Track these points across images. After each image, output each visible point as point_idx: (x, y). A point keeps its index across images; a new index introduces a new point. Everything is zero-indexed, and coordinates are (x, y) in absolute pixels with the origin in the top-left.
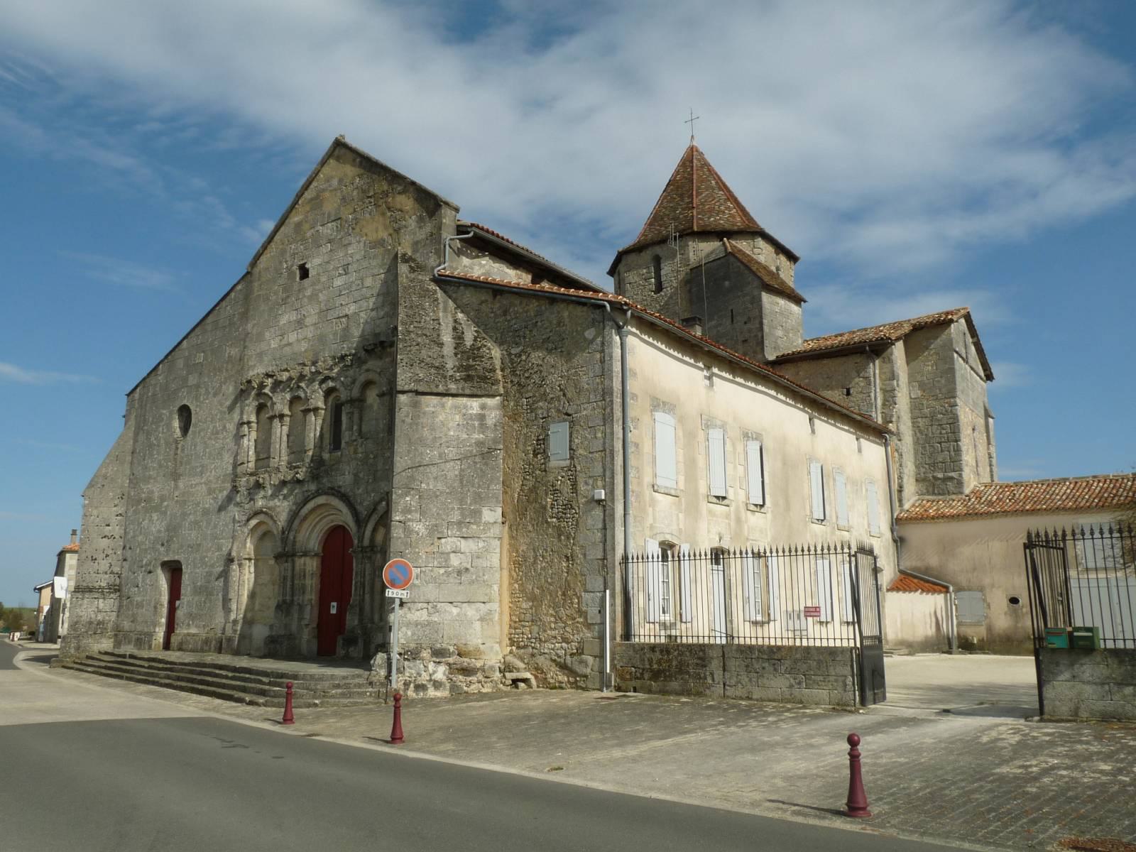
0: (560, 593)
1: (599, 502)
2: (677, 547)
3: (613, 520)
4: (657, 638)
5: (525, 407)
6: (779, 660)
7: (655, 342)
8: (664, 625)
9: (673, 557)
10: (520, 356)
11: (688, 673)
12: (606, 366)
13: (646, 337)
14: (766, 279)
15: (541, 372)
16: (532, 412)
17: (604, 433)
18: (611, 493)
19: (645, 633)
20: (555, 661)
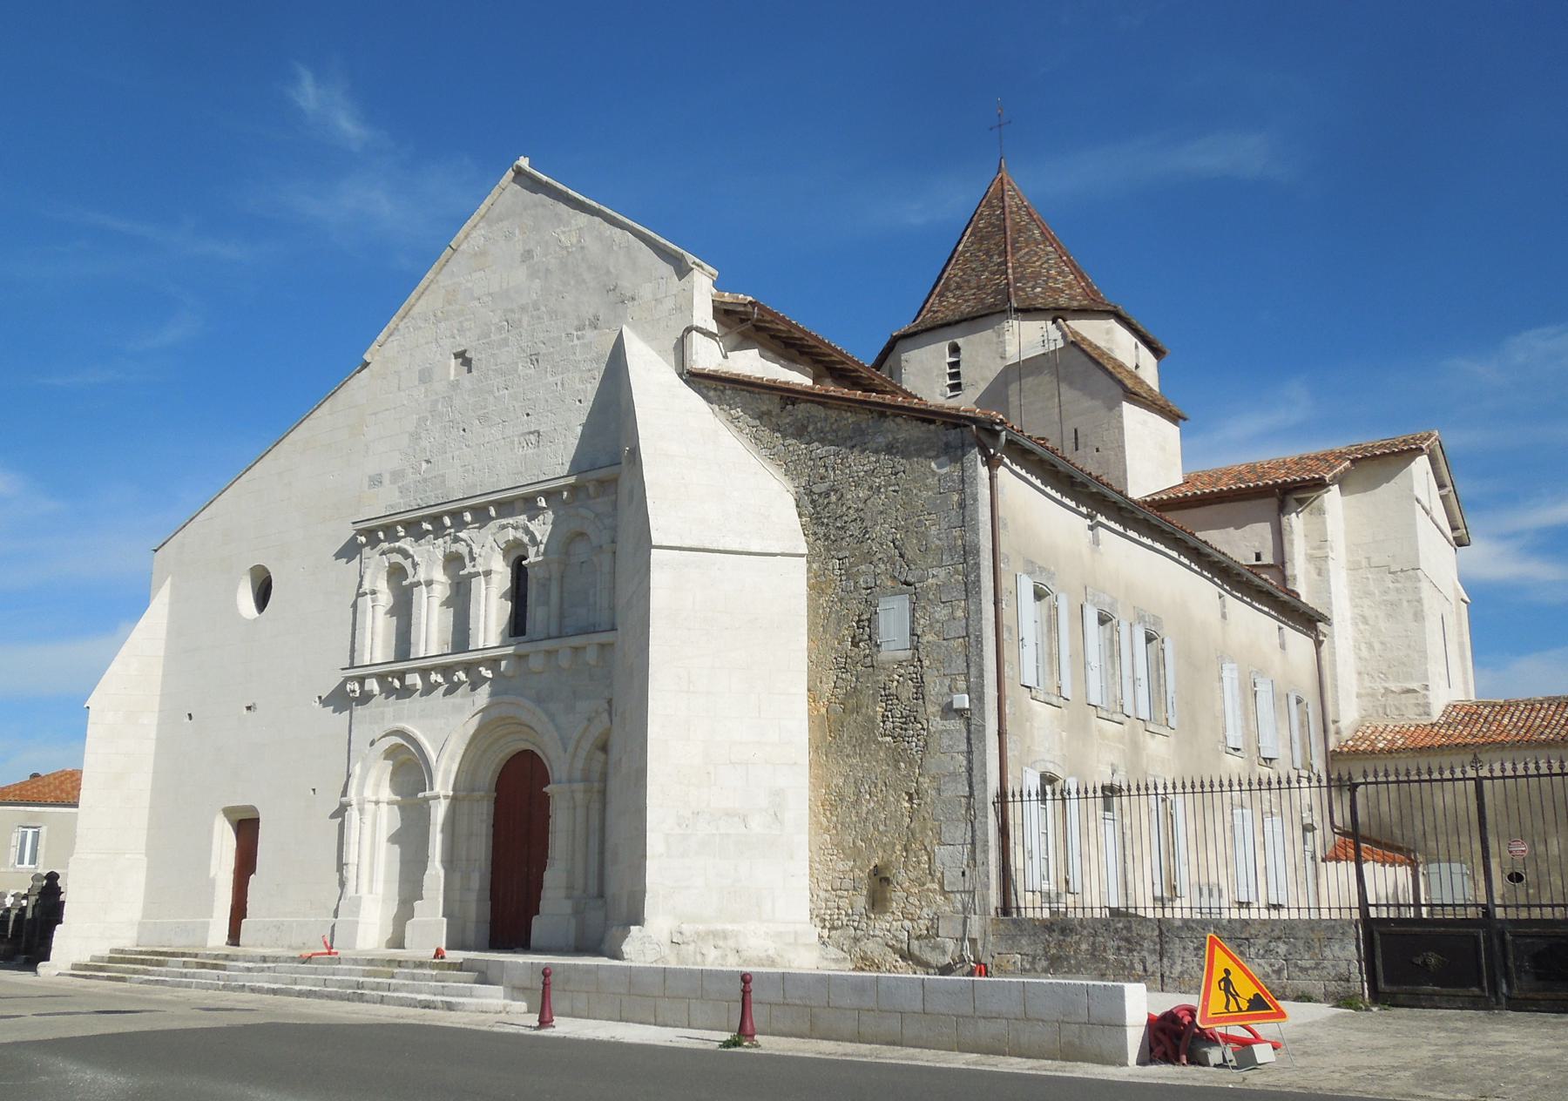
0: (898, 847)
1: (960, 712)
2: (1061, 782)
3: (983, 739)
4: (1038, 910)
5: (837, 572)
6: (1247, 939)
7: (1028, 476)
8: (1047, 896)
9: (1054, 793)
10: (828, 495)
11: (1105, 960)
12: (967, 513)
13: (1017, 468)
14: (1129, 383)
15: (862, 520)
16: (848, 579)
17: (966, 610)
18: (978, 697)
19: (1031, 906)
20: (891, 947)
